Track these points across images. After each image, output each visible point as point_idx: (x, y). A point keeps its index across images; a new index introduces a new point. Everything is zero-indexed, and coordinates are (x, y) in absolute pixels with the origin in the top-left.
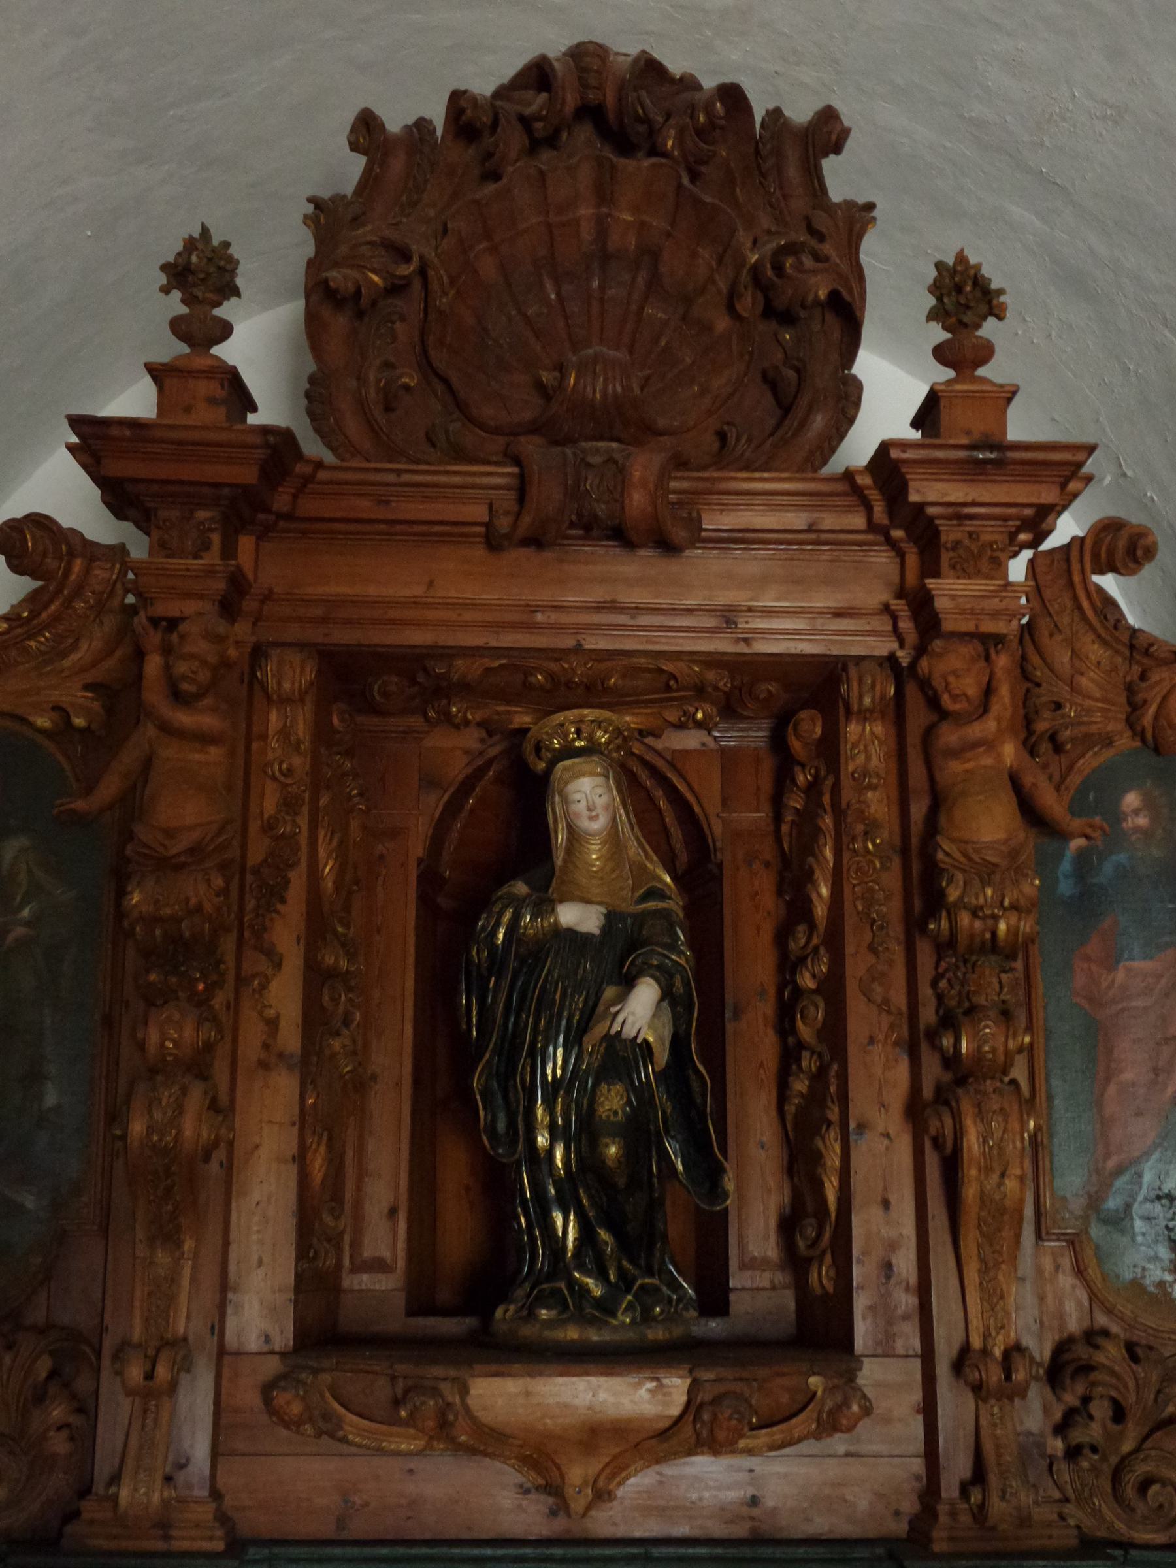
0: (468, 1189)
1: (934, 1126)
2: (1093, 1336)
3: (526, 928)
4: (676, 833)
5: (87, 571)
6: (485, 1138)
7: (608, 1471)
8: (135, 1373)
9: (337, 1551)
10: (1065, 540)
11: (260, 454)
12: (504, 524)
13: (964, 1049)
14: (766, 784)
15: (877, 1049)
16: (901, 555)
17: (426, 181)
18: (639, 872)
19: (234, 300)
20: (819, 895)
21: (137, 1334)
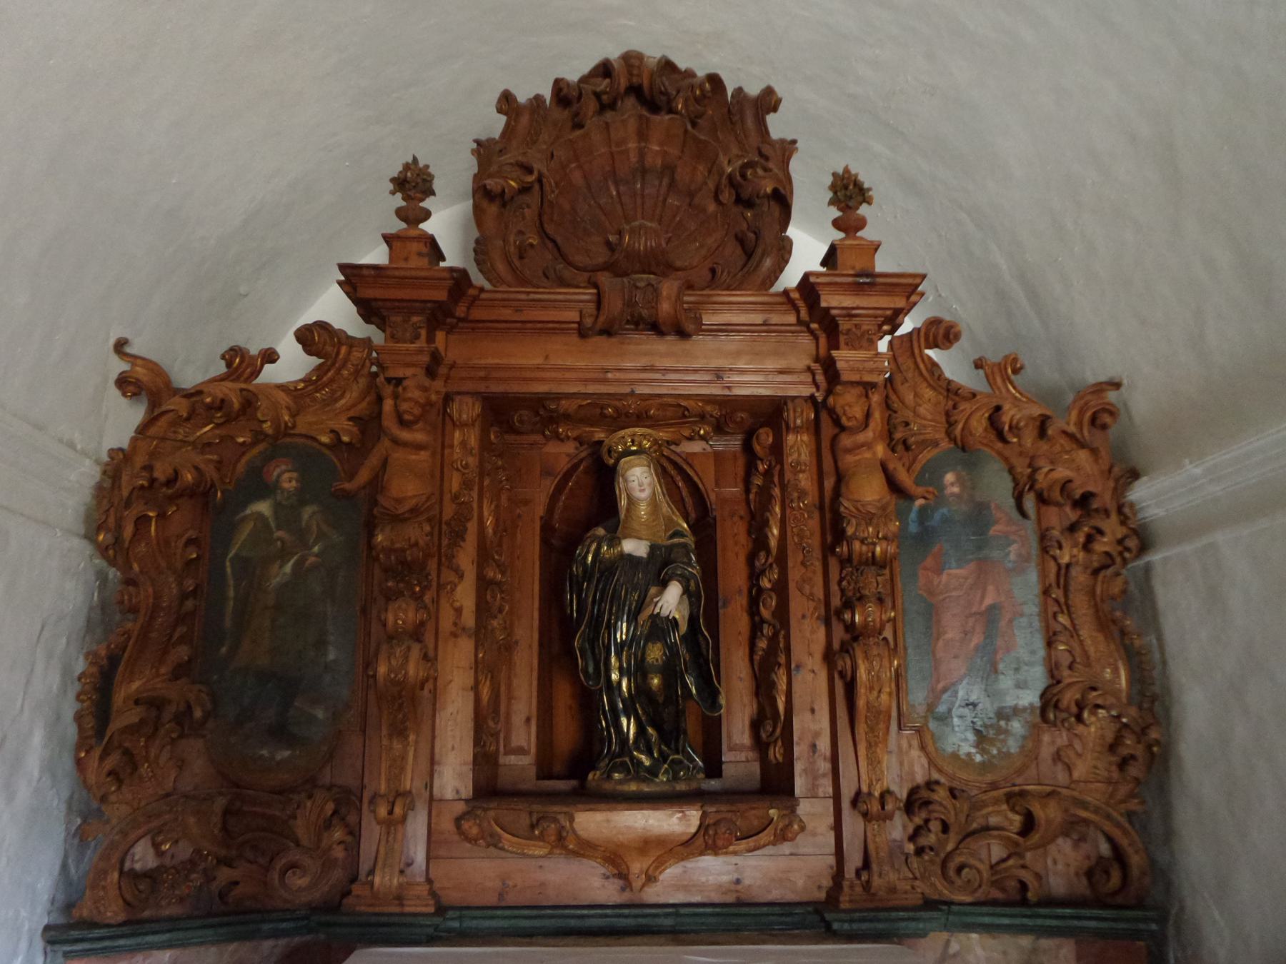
0: (570, 708)
1: (840, 664)
2: (930, 785)
3: (604, 554)
4: (688, 500)
5: (349, 353)
6: (581, 675)
7: (654, 865)
8: (383, 811)
9: (499, 912)
10: (909, 330)
11: (450, 282)
12: (588, 322)
13: (857, 620)
14: (741, 471)
15: (807, 621)
16: (816, 338)
17: (541, 129)
18: (669, 522)
19: (432, 198)
20: (773, 534)
21: (383, 788)
